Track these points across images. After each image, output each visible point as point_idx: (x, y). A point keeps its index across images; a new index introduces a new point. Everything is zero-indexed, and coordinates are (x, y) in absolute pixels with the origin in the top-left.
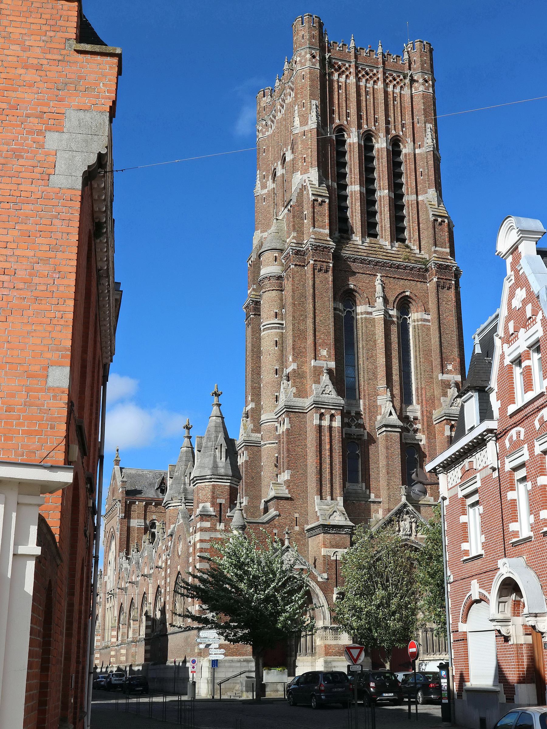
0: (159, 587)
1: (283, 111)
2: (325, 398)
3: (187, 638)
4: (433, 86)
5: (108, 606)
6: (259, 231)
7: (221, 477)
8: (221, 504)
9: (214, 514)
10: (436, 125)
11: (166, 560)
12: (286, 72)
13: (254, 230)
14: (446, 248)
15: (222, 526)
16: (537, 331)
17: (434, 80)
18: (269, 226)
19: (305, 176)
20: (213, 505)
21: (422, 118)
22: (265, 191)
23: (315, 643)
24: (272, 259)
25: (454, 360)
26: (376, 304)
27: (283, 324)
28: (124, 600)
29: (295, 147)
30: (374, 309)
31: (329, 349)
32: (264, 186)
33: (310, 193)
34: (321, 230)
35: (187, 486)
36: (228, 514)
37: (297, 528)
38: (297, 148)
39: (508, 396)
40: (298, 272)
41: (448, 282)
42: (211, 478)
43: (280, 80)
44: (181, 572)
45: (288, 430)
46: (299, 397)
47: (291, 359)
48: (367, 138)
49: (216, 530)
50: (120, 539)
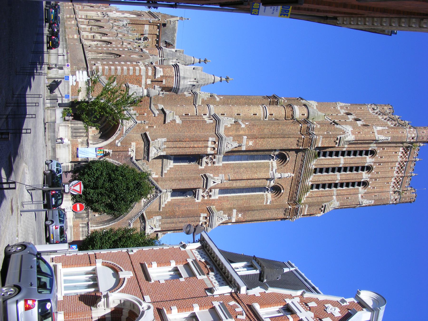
0: (111, 43)
1: (383, 119)
2: (224, 144)
3: (81, 61)
4: (393, 204)
5: (99, 13)
6: (317, 104)
7: (178, 82)
8: (162, 82)
9: (156, 78)
10: (373, 205)
11: (128, 48)
12: (403, 122)
13: (318, 102)
14: (307, 212)
15: (149, 82)
16: (301, 312)
17: (396, 203)
18: (320, 110)
19: (350, 133)
20: (162, 77)
21: (377, 198)
22: (339, 108)
23: (79, 138)
24: (303, 112)
25: (244, 218)
26: (277, 173)
27: (266, 118)
28: (102, 22)
29: (366, 127)
30: (274, 172)
31: (253, 147)
32: (342, 107)
33: (341, 136)
34: (321, 142)
35: (171, 61)
36: (156, 86)
37: (147, 127)
38: (365, 129)
39: (265, 301)
40: (297, 128)
41: (288, 214)
42: (178, 76)
43: (398, 118)
44: (120, 57)
45: (206, 121)
46: (225, 129)
47: (247, 123)
48: (369, 169)
49: (146, 78)
50: (137, 20)
